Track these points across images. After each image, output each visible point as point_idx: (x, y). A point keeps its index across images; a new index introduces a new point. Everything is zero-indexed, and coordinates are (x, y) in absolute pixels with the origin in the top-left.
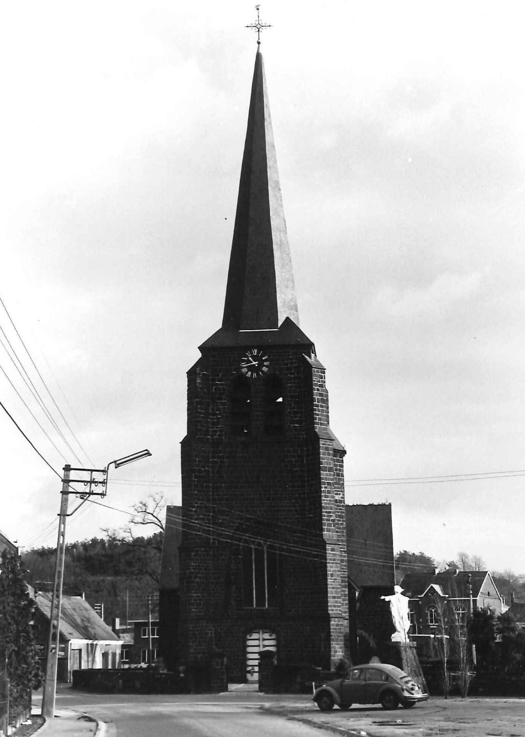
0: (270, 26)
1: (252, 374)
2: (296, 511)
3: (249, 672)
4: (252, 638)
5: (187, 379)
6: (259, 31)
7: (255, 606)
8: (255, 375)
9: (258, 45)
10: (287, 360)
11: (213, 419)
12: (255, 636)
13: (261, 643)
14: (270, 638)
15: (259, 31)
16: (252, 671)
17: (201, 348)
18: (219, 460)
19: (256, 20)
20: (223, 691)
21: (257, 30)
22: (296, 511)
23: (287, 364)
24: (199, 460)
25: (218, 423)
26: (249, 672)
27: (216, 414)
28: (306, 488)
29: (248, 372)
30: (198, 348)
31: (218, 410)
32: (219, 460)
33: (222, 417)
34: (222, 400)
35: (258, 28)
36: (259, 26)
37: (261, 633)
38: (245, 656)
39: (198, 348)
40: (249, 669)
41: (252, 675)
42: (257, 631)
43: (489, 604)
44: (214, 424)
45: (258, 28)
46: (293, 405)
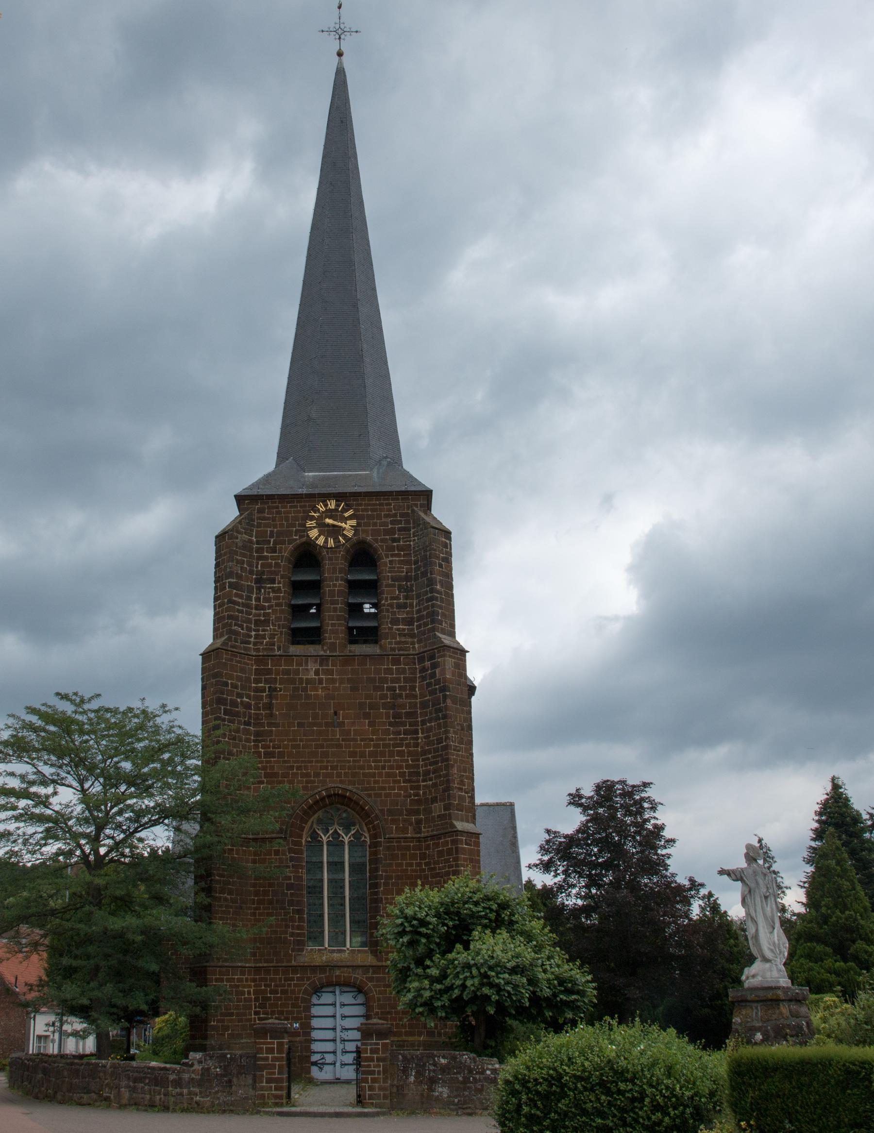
0: (357, 32)
1: (326, 542)
2: (402, 774)
3: (315, 1064)
4: (321, 1002)
5: (214, 548)
6: (340, 38)
7: (327, 946)
8: (331, 543)
9: (337, 58)
10: (386, 516)
11: (259, 615)
12: (327, 998)
13: (339, 1011)
14: (354, 1002)
15: (340, 38)
16: (321, 1062)
17: (241, 499)
18: (267, 686)
19: (336, 23)
20: (312, 643)
21: (337, 37)
22: (402, 774)
23: (386, 524)
24: (231, 683)
25: (266, 622)
26: (315, 1064)
27: (264, 608)
28: (420, 735)
29: (319, 536)
30: (235, 496)
31: (267, 600)
32: (267, 686)
33: (274, 612)
34: (275, 583)
35: (340, 33)
36: (340, 32)
37: (337, 992)
38: (309, 1034)
39: (235, 496)
40: (315, 1058)
41: (321, 1069)
42: (331, 989)
43: (811, 829)
44: (258, 623)
45: (340, 33)
46: (397, 593)
